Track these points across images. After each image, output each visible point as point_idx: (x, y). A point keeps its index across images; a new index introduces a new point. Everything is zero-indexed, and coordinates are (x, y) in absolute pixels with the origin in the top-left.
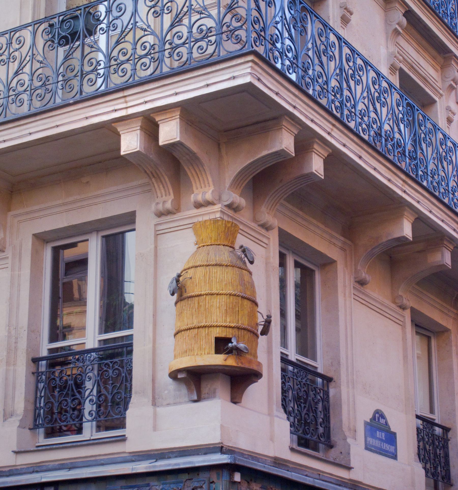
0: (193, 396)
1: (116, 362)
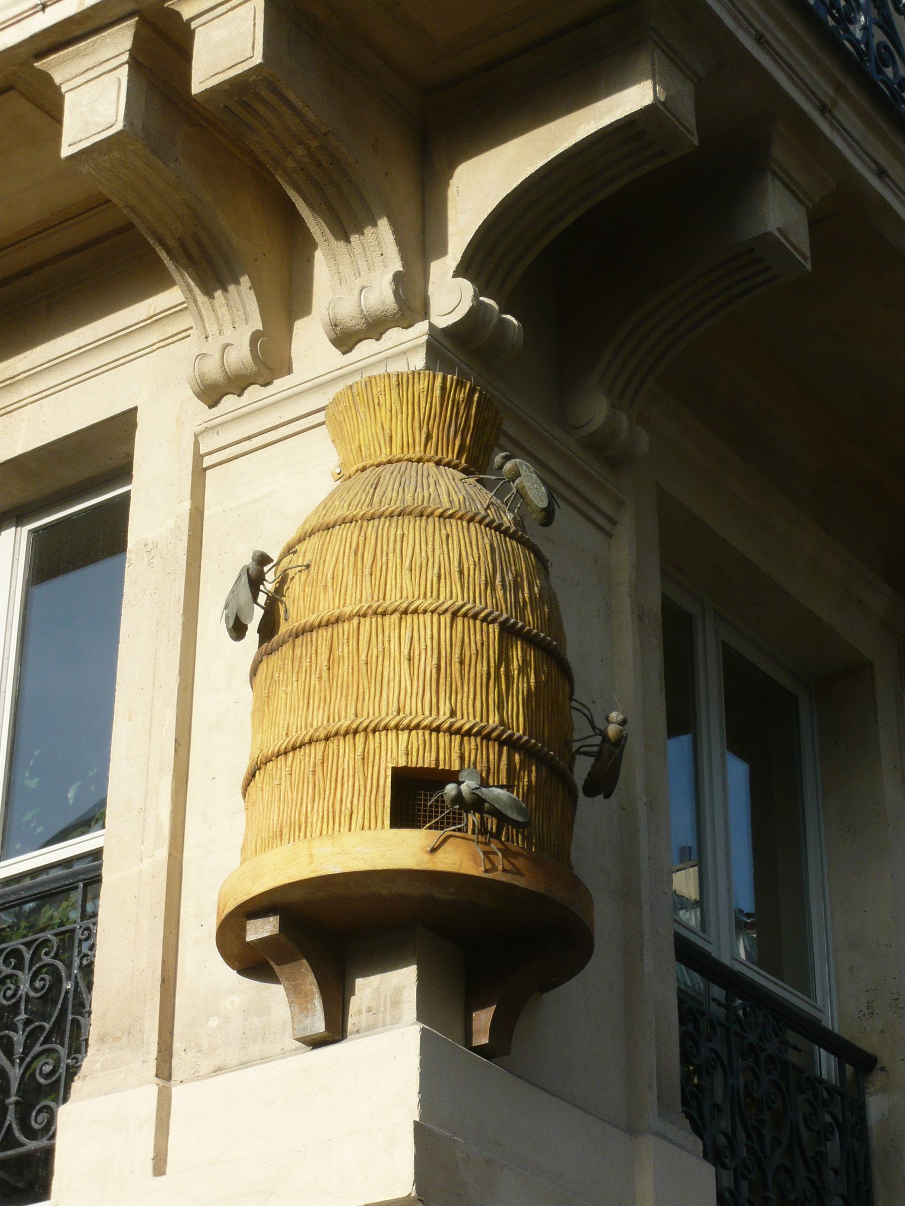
0: (308, 1022)
1: (46, 942)
